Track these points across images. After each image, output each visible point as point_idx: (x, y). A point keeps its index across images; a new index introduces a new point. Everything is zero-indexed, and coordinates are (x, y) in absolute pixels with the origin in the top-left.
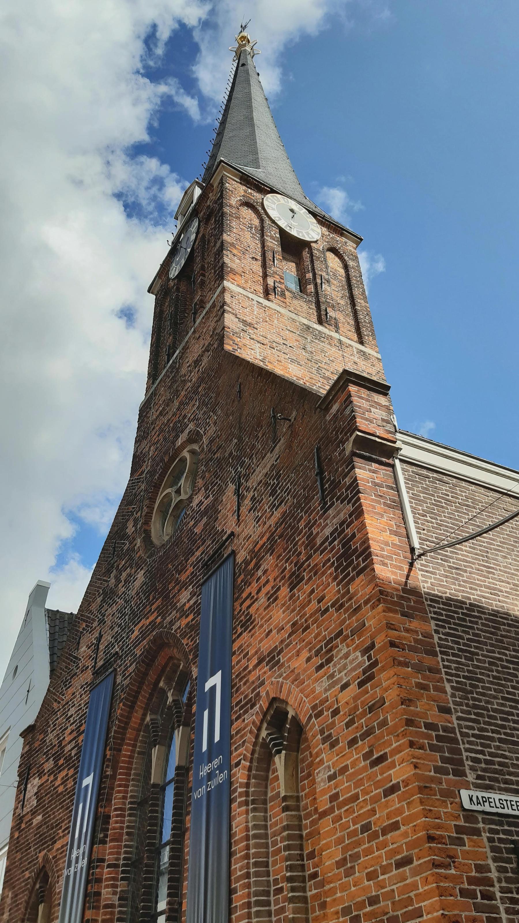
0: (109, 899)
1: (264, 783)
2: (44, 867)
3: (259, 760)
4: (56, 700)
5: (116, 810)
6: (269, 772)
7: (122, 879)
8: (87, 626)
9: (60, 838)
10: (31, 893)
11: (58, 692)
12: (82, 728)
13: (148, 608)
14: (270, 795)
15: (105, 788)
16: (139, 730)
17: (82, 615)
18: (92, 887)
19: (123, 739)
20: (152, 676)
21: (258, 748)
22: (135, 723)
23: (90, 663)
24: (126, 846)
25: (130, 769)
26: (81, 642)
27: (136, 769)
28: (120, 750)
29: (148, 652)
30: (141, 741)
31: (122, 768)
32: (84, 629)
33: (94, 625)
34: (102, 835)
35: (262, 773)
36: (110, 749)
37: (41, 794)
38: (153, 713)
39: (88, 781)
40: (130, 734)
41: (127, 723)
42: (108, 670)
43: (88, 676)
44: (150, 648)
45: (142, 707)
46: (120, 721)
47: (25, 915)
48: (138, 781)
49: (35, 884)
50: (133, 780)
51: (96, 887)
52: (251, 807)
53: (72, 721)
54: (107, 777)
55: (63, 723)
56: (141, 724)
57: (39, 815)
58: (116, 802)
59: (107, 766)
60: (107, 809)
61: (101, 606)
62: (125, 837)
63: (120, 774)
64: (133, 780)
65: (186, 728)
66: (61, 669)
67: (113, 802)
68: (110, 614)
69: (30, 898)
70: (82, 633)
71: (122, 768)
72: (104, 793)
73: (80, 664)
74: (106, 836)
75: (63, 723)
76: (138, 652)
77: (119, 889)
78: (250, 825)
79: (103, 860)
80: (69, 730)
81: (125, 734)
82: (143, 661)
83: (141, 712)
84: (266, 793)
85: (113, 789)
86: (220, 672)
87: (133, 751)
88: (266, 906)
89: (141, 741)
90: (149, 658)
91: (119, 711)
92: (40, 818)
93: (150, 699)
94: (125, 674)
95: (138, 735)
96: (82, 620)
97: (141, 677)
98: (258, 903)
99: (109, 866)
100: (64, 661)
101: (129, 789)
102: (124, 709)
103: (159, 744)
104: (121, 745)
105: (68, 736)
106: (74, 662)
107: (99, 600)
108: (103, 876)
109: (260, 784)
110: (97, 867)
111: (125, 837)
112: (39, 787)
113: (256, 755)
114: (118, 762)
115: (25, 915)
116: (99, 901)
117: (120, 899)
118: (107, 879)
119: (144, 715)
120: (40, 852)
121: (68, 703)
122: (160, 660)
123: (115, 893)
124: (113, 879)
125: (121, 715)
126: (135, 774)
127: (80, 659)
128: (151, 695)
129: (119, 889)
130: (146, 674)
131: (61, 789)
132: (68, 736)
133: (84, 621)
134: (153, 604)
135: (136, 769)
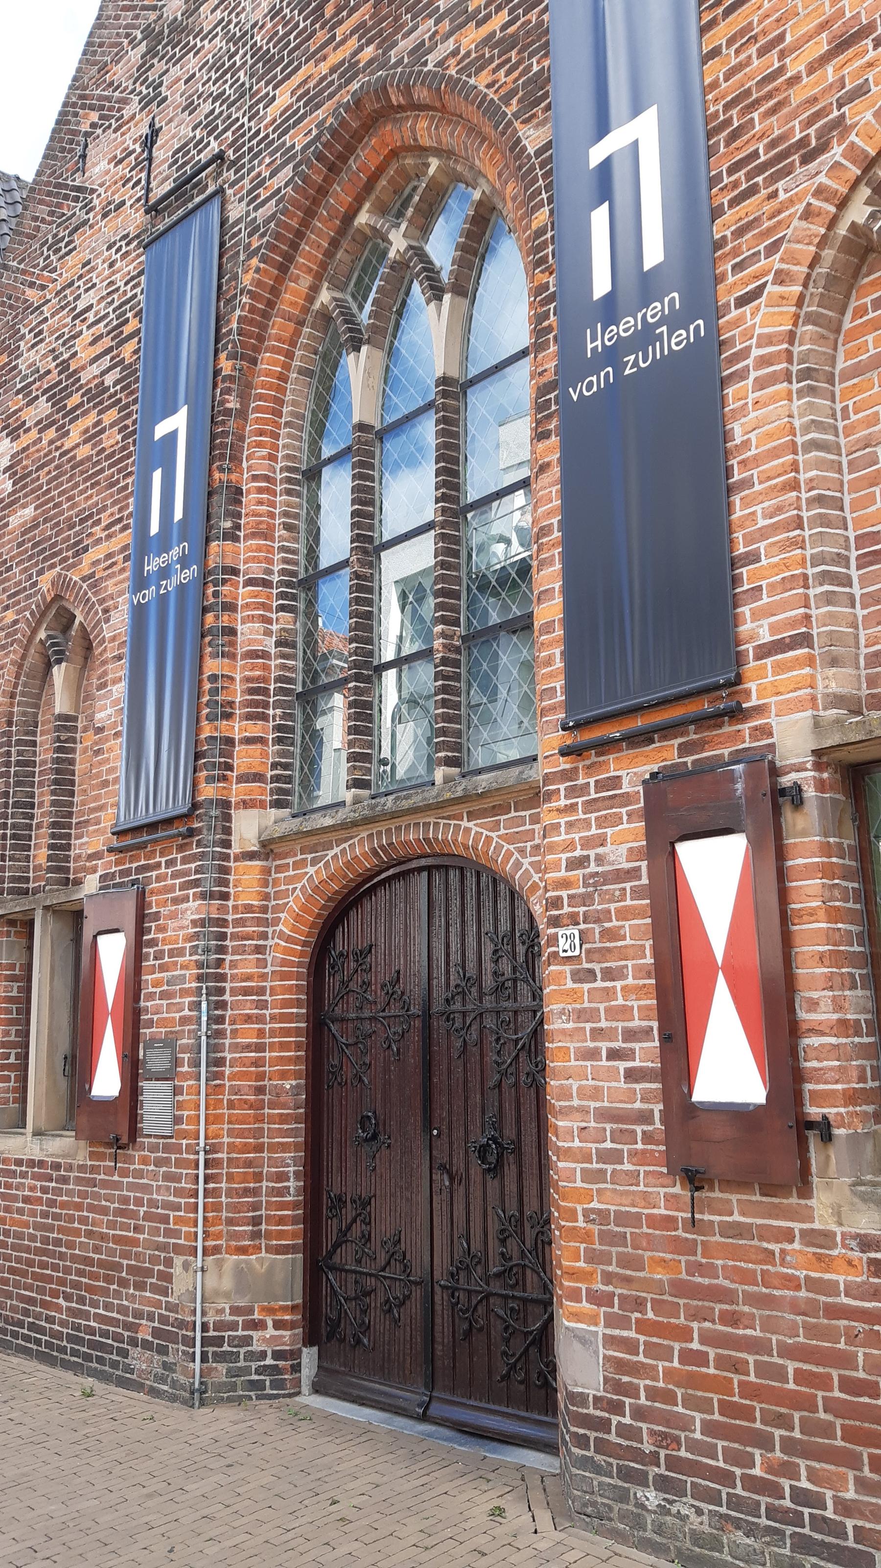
0: (260, 642)
1: (832, 337)
2: (58, 597)
3: (831, 281)
4: (32, 285)
5: (255, 478)
6: (843, 314)
7: (282, 608)
8: (101, 118)
9: (99, 541)
10: (26, 649)
11: (34, 267)
12: (127, 330)
13: (322, 36)
14: (840, 365)
15: (225, 434)
16: (301, 323)
17: (82, 97)
18: (217, 617)
19: (261, 339)
20: (339, 196)
21: (829, 254)
22: (293, 304)
23: (131, 194)
24: (283, 549)
25: (281, 402)
26: (91, 152)
27: (294, 403)
28: (254, 361)
29: (334, 133)
30: (306, 347)
31: (261, 397)
32: (94, 125)
33: (127, 113)
34: (228, 524)
35: (830, 313)
36: (232, 356)
37: (26, 467)
38: (336, 286)
39: (177, 423)
40: (277, 327)
41: (271, 304)
42: (192, 198)
43: (134, 219)
44: (343, 123)
45: (310, 270)
46: (253, 295)
47: (16, 686)
48: (301, 429)
49: (34, 631)
50: (287, 424)
51: (226, 618)
52: (795, 386)
53: (92, 320)
54: (228, 412)
55: (65, 326)
56: (306, 310)
57: (24, 506)
58: (254, 461)
59: (228, 391)
60: (234, 477)
61: (144, 67)
62: (280, 532)
63: (258, 409)
64: (287, 424)
65: (459, 299)
66: (35, 219)
67: (245, 465)
68: (178, 79)
69: (24, 657)
70: (87, 134)
71: (261, 397)
72: (223, 446)
73: (96, 202)
74: (238, 527)
75: (65, 326)
76: (297, 139)
77: (275, 627)
78: (797, 423)
79: (235, 572)
80: (87, 335)
81: (264, 327)
82: (320, 157)
83: (306, 281)
84: (833, 360)
85: (242, 439)
86: (157, 437)
87: (287, 367)
88: (844, 586)
89: (306, 347)
90: (335, 151)
91: (251, 275)
92: (29, 512)
93: (329, 254)
94: (253, 202)
95: (297, 333)
96: (83, 107)
97: (311, 198)
98: (825, 578)
99: (250, 582)
100: (41, 202)
101: (281, 443)
102: (265, 271)
103: (368, 342)
104: (257, 349)
105: (85, 348)
106: (76, 199)
107: (135, 55)
108: (236, 599)
109: (823, 337)
110: (224, 582)
111: (280, 532)
112: (13, 457)
113: (822, 270)
114: (249, 386)
115: (16, 686)
116: (233, 644)
117: (278, 644)
118: (247, 606)
119: (315, 289)
120: (40, 573)
121: (71, 284)
122: (366, 157)
123: (268, 633)
124: (264, 606)
125: (259, 284)
126: (292, 414)
127: (93, 191)
128: (335, 243)
129: (275, 627)
130: (322, 191)
131: (84, 451)
132: (85, 348)
133: (92, 108)
134: (340, 22)
135: (294, 403)
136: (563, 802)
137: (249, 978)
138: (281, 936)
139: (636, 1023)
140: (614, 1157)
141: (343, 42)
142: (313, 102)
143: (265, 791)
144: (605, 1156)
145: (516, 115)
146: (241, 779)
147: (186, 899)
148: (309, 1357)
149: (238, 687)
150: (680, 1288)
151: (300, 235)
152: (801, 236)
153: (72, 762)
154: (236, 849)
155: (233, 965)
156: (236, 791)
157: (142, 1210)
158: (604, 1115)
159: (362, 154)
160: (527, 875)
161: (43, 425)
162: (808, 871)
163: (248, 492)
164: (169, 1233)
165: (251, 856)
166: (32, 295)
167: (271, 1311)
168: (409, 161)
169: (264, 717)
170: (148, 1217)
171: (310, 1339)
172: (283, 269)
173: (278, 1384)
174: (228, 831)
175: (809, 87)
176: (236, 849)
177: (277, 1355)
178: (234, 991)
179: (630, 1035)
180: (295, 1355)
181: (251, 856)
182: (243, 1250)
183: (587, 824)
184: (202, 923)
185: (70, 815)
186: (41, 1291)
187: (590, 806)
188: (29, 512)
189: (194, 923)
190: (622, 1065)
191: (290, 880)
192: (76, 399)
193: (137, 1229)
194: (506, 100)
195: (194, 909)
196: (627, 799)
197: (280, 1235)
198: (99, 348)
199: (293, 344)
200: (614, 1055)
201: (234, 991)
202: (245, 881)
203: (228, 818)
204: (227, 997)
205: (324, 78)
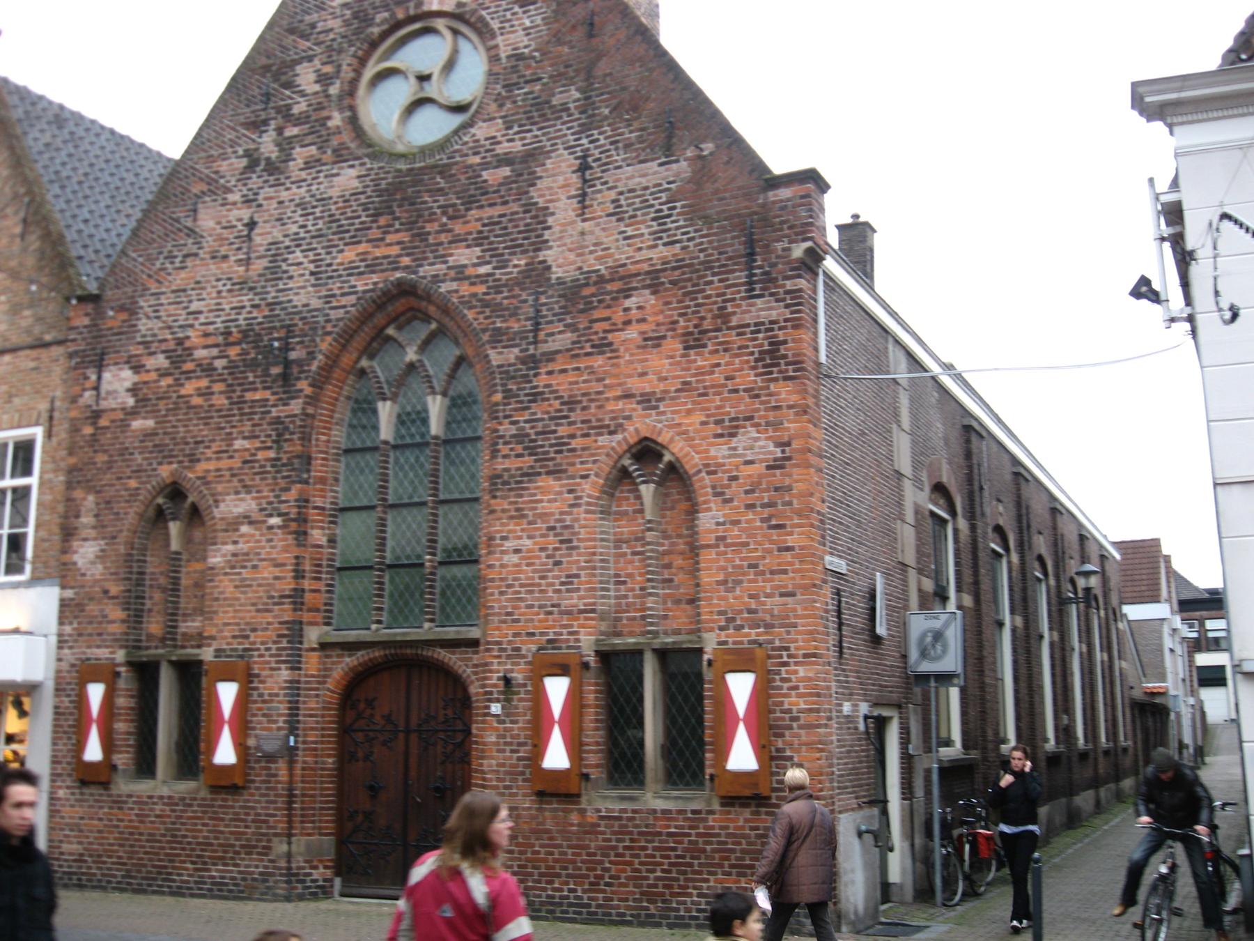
9: (209, 459)
40: (337, 373)
56: (353, 367)
76: (361, 285)
83: (355, 355)
130: (371, 315)
131: (196, 401)
136: (496, 653)
137: (312, 709)
138: (329, 690)
139: (522, 740)
140: (509, 787)
141: (390, 245)
142: (372, 268)
143: (319, 617)
144: (506, 787)
145: (489, 342)
146: (310, 610)
147: (279, 669)
148: (338, 882)
149: (307, 562)
150: (534, 831)
151: (355, 331)
152: (605, 464)
153: (179, 578)
154: (306, 646)
155: (305, 702)
156: (306, 617)
157: (250, 818)
158: (507, 773)
159: (397, 304)
160: (469, 676)
161: (164, 374)
162: (590, 692)
163: (316, 459)
164: (269, 828)
165: (313, 650)
166: (154, 288)
167: (321, 861)
168: (634, 721)
169: (319, 579)
170: (253, 821)
171: (338, 874)
172: (344, 346)
173: (324, 893)
174: (301, 636)
175: (611, 406)
176: (306, 646)
177: (325, 880)
178: (305, 716)
179: (520, 744)
180: (331, 880)
181: (313, 650)
182: (309, 835)
183: (506, 663)
184: (290, 682)
185: (177, 609)
186: (171, 861)
187: (509, 657)
188: (150, 423)
189: (286, 681)
190: (515, 755)
191: (333, 663)
192: (189, 366)
193: (246, 827)
194: (484, 331)
195: (285, 674)
196: (524, 657)
197: (327, 828)
198: (210, 341)
199: (343, 382)
200: (512, 751)
201: (305, 716)
202: (312, 663)
203: (301, 630)
204: (301, 718)
205: (377, 258)
